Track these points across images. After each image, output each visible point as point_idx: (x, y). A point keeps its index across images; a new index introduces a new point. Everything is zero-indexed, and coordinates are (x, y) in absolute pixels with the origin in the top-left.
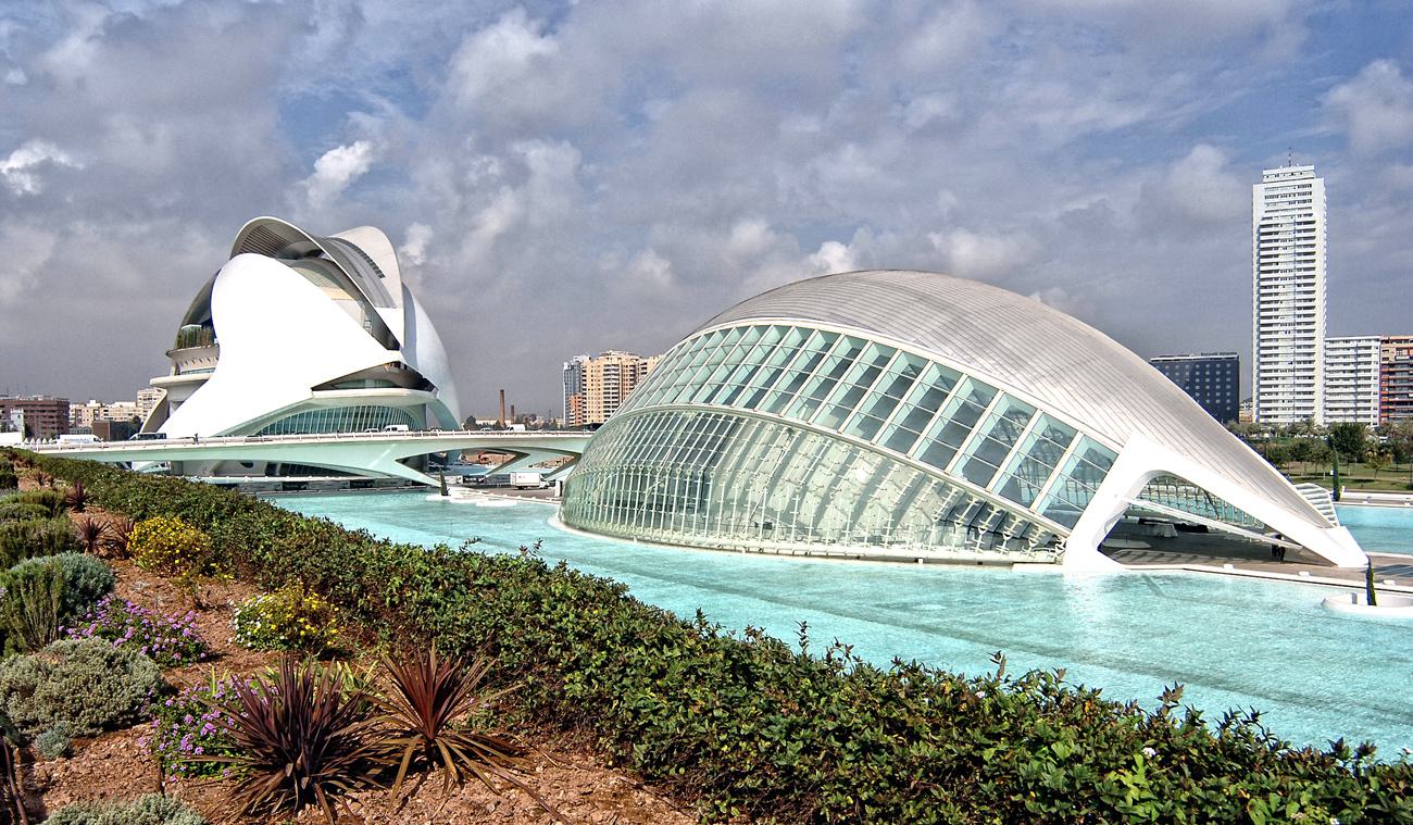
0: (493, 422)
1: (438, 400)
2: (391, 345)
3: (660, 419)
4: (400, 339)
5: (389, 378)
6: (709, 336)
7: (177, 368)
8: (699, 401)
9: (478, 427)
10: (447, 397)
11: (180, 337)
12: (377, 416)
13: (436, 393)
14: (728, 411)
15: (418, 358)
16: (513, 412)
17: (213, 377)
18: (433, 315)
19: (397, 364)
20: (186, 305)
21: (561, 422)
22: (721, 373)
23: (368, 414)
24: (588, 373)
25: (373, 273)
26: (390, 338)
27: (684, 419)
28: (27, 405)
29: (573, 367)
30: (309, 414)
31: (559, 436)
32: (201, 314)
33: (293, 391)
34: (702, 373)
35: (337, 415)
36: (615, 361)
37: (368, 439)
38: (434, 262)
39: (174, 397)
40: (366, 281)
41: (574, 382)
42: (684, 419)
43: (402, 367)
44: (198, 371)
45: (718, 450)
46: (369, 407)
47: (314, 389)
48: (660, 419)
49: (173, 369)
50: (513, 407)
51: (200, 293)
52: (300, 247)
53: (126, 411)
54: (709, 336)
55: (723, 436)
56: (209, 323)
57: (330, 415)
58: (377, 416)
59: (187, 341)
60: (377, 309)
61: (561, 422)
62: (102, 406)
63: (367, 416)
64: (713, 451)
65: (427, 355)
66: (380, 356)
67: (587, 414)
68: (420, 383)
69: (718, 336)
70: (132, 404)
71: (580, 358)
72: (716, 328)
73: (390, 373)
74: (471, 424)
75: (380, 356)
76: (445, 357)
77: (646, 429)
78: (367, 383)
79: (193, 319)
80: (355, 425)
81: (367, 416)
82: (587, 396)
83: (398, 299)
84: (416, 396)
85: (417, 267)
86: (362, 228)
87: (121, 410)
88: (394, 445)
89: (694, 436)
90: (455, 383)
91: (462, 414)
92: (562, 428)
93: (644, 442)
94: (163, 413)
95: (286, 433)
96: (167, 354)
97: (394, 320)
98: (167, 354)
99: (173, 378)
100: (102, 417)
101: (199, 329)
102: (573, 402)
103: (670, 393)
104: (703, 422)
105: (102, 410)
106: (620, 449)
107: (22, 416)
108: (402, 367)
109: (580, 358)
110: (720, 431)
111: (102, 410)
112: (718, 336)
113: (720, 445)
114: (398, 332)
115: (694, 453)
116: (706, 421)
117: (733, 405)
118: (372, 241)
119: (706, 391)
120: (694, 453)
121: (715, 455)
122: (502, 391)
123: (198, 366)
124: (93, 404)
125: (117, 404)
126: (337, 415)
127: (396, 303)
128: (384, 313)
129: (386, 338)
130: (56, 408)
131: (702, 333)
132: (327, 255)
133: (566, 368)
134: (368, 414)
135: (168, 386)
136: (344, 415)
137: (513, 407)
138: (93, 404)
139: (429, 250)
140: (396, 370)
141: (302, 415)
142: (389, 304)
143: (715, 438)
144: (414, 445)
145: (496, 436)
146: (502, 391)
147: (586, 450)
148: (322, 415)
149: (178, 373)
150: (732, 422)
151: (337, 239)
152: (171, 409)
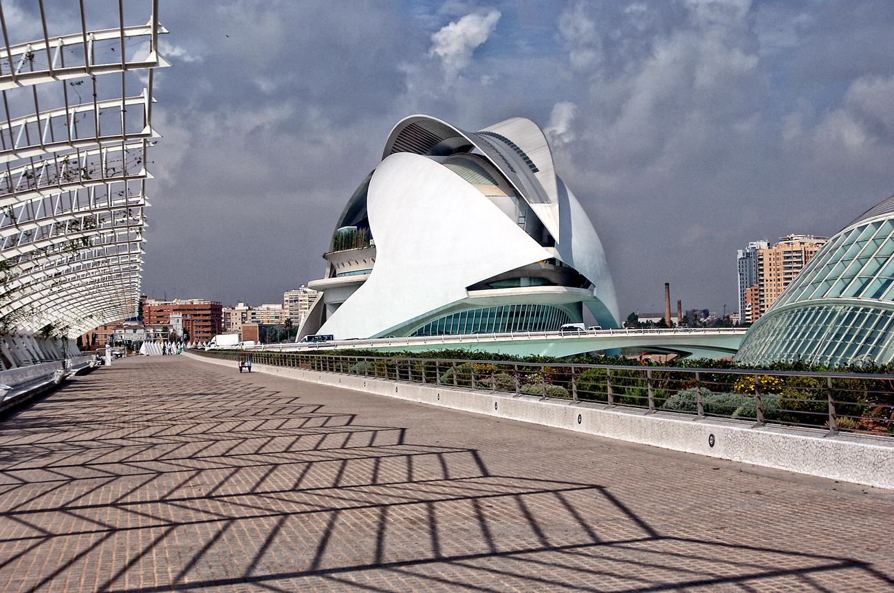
0: (656, 320)
1: (595, 297)
2: (545, 240)
3: (818, 313)
4: (556, 235)
5: (544, 275)
6: (862, 228)
7: (332, 267)
8: (848, 295)
9: (639, 326)
10: (606, 296)
11: (336, 239)
12: (533, 315)
13: (592, 291)
14: (856, 303)
15: (573, 254)
16: (680, 308)
17: (371, 279)
18: (580, 199)
19: (552, 261)
20: (342, 204)
21: (737, 318)
22: (870, 265)
23: (523, 313)
24: (766, 262)
25: (526, 167)
26: (545, 234)
27: (834, 313)
28: (183, 310)
29: (748, 255)
30: (463, 315)
31: (722, 333)
32: (357, 214)
33: (448, 291)
34: (851, 266)
35: (492, 315)
36: (797, 247)
37: (509, 339)
38: (587, 136)
39: (331, 299)
40: (520, 178)
41: (750, 272)
42: (834, 313)
43: (558, 264)
44: (353, 273)
45: (865, 343)
46: (524, 306)
47: (469, 289)
48: (818, 313)
49: (328, 270)
50: (679, 303)
51: (355, 194)
52: (450, 143)
53: (272, 314)
54: (862, 228)
55: (882, 331)
56: (365, 224)
57: (485, 315)
58: (533, 315)
59: (343, 243)
60: (531, 205)
61: (737, 318)
62: (250, 309)
63: (523, 315)
64: (861, 344)
65: (584, 251)
66: (535, 253)
67: (765, 304)
68: (572, 278)
69: (869, 229)
70: (279, 307)
71: (756, 244)
72: (868, 221)
73: (545, 270)
74: (632, 322)
75: (535, 253)
76: (602, 252)
77: (796, 324)
78: (523, 281)
79: (347, 221)
80: (510, 325)
81: (523, 315)
82: (765, 288)
83: (553, 194)
84: (573, 294)
85: (566, 145)
86: (517, 119)
87: (270, 312)
88: (551, 345)
89: (842, 329)
90: (614, 280)
91: (621, 310)
92: (737, 325)
93: (802, 336)
94: (319, 316)
95: (441, 333)
96: (324, 257)
97: (549, 215)
98: (324, 257)
99: (328, 281)
100: (249, 323)
101: (355, 229)
102: (749, 295)
103: (837, 284)
104: (852, 315)
105: (249, 313)
106: (778, 343)
107: (180, 320)
108: (558, 264)
109: (756, 244)
110: (867, 324)
111: (249, 313)
112: (869, 229)
113: (879, 340)
114: (553, 228)
115: (842, 346)
116: (855, 314)
117: (860, 296)
118: (516, 130)
119: (855, 285)
120: (842, 346)
121: (862, 347)
122: (667, 284)
123: (354, 268)
124: (241, 307)
125: (265, 306)
126: (492, 315)
127: (550, 198)
128: (538, 208)
129: (540, 234)
130: (209, 312)
131: (855, 226)
132: (478, 150)
133: (740, 255)
134: (523, 313)
135: (325, 289)
136: (499, 315)
137: (679, 303)
138: (241, 307)
139: (576, 125)
140: (551, 267)
141: (456, 316)
142: (543, 199)
143: (862, 332)
144: (576, 344)
145: (656, 334)
146: (667, 284)
147: (741, 347)
148: (478, 316)
149: (334, 275)
150: (880, 315)
151: (483, 133)
152: (328, 311)
